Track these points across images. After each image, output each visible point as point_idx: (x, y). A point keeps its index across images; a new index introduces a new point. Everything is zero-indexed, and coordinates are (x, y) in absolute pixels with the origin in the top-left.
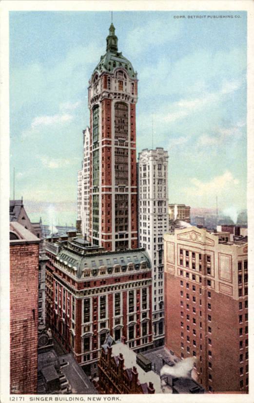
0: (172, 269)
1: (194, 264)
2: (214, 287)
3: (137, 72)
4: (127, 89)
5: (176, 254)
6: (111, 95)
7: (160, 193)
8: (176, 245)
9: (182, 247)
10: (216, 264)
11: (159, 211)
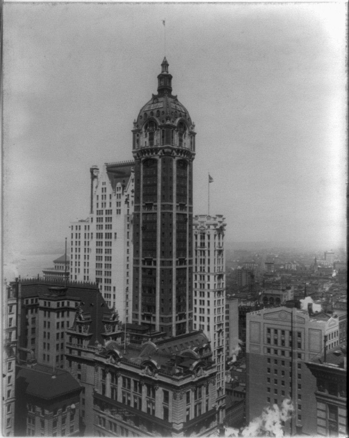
0: (256, 349)
1: (283, 342)
2: (305, 358)
3: (195, 124)
4: (187, 141)
5: (262, 333)
6: (174, 151)
7: (78, 240)
8: (262, 324)
9: (270, 326)
10: (307, 339)
11: (201, 287)
